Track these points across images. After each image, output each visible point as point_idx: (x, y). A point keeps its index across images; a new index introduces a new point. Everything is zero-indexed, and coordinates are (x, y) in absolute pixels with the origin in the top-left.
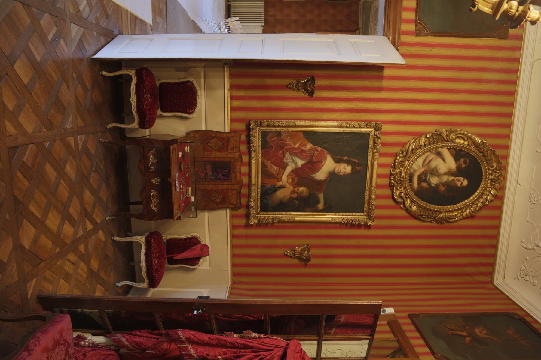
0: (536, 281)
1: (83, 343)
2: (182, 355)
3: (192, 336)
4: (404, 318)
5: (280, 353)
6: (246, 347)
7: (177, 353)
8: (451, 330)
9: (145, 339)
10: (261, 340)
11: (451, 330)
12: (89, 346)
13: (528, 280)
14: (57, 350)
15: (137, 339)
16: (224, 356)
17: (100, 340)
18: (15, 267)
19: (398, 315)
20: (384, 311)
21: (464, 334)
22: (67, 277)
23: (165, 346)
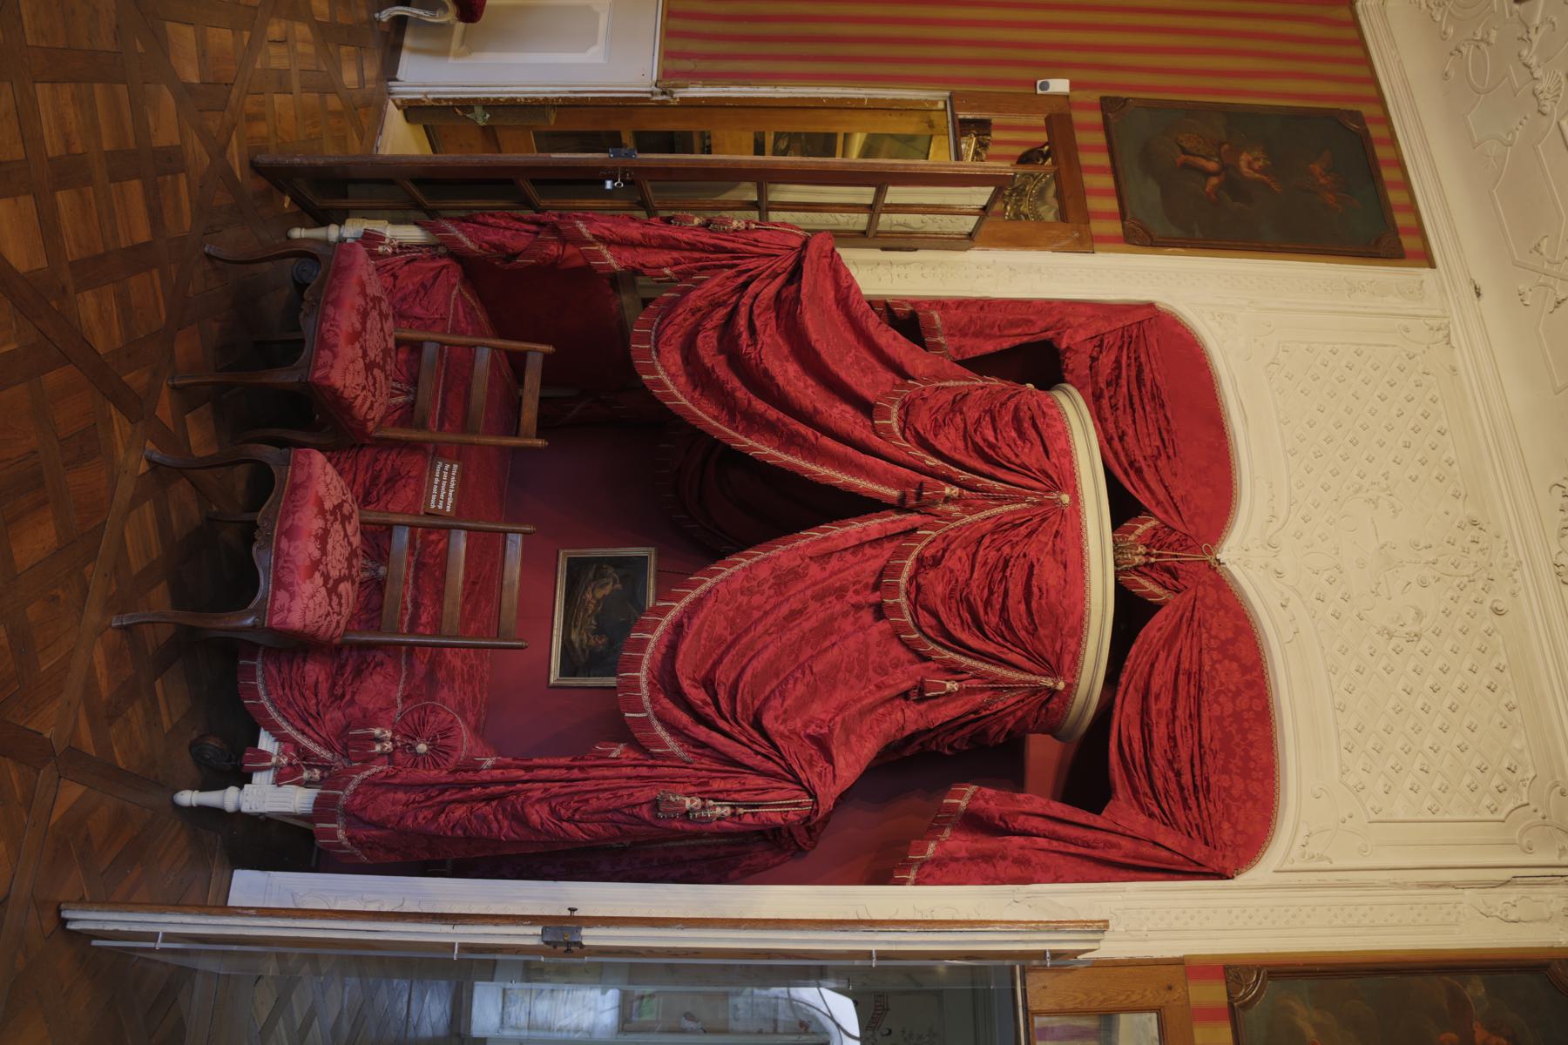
0: (1451, 31)
1: (380, 249)
2: (590, 266)
3: (607, 233)
5: (788, 263)
6: (718, 249)
7: (580, 262)
8: (1184, 151)
9: (508, 233)
10: (751, 236)
11: (1184, 151)
12: (394, 253)
13: (1438, 18)
14: (368, 325)
15: (493, 237)
17: (412, 234)
18: (196, 139)
19: (1080, 96)
20: (1045, 86)
21: (1212, 165)
22: (282, 85)
23: (554, 249)
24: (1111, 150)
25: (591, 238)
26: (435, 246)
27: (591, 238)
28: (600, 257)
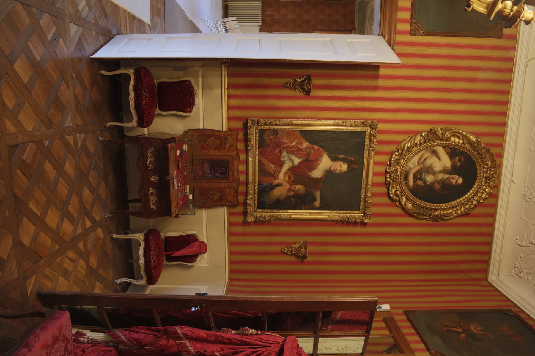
0: (530, 278)
1: (82, 339)
2: (180, 351)
3: (190, 333)
4: (400, 314)
5: (277, 349)
6: (243, 343)
7: (175, 349)
8: (445, 326)
10: (259, 337)
11: (445, 326)
12: (88, 343)
13: (522, 277)
14: (56, 346)
15: (136, 336)
16: (221, 352)
17: (99, 336)
18: (15, 264)
19: (394, 311)
20: (380, 308)
21: (459, 330)
22: (66, 274)
23: (163, 342)
24: (414, 327)
25: (182, 335)
26: (108, 342)
27: (182, 335)
28: (185, 346)
